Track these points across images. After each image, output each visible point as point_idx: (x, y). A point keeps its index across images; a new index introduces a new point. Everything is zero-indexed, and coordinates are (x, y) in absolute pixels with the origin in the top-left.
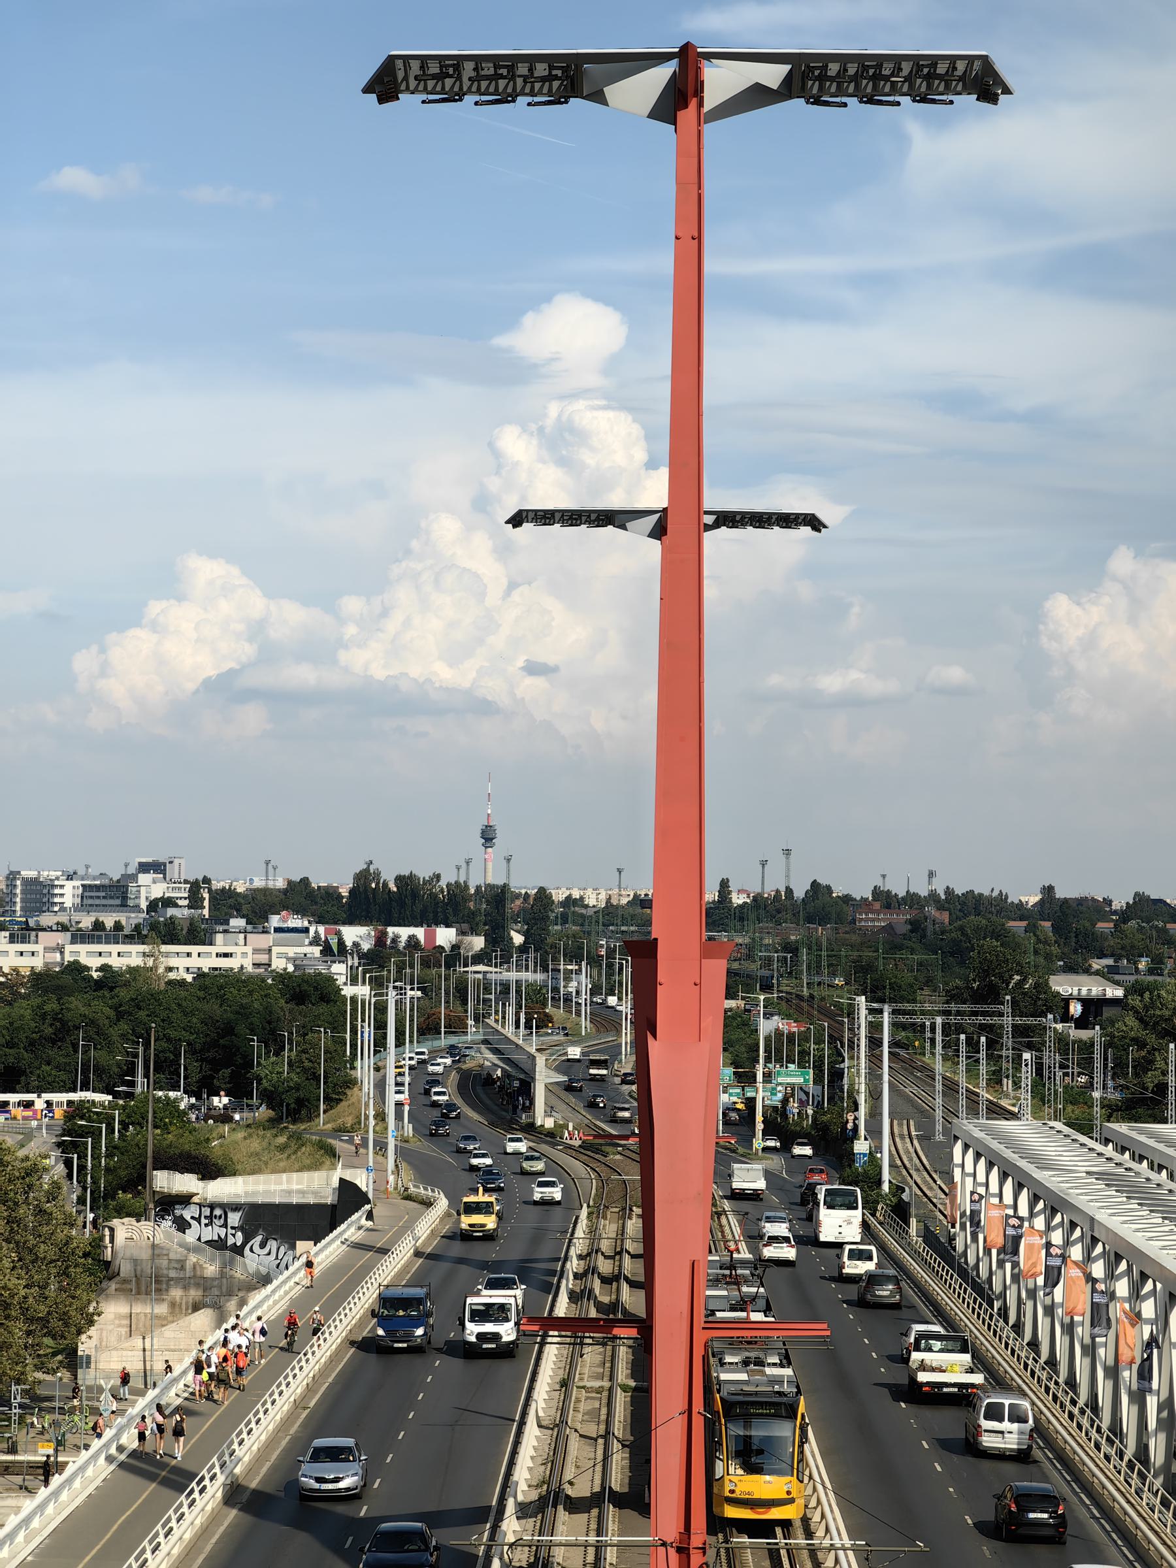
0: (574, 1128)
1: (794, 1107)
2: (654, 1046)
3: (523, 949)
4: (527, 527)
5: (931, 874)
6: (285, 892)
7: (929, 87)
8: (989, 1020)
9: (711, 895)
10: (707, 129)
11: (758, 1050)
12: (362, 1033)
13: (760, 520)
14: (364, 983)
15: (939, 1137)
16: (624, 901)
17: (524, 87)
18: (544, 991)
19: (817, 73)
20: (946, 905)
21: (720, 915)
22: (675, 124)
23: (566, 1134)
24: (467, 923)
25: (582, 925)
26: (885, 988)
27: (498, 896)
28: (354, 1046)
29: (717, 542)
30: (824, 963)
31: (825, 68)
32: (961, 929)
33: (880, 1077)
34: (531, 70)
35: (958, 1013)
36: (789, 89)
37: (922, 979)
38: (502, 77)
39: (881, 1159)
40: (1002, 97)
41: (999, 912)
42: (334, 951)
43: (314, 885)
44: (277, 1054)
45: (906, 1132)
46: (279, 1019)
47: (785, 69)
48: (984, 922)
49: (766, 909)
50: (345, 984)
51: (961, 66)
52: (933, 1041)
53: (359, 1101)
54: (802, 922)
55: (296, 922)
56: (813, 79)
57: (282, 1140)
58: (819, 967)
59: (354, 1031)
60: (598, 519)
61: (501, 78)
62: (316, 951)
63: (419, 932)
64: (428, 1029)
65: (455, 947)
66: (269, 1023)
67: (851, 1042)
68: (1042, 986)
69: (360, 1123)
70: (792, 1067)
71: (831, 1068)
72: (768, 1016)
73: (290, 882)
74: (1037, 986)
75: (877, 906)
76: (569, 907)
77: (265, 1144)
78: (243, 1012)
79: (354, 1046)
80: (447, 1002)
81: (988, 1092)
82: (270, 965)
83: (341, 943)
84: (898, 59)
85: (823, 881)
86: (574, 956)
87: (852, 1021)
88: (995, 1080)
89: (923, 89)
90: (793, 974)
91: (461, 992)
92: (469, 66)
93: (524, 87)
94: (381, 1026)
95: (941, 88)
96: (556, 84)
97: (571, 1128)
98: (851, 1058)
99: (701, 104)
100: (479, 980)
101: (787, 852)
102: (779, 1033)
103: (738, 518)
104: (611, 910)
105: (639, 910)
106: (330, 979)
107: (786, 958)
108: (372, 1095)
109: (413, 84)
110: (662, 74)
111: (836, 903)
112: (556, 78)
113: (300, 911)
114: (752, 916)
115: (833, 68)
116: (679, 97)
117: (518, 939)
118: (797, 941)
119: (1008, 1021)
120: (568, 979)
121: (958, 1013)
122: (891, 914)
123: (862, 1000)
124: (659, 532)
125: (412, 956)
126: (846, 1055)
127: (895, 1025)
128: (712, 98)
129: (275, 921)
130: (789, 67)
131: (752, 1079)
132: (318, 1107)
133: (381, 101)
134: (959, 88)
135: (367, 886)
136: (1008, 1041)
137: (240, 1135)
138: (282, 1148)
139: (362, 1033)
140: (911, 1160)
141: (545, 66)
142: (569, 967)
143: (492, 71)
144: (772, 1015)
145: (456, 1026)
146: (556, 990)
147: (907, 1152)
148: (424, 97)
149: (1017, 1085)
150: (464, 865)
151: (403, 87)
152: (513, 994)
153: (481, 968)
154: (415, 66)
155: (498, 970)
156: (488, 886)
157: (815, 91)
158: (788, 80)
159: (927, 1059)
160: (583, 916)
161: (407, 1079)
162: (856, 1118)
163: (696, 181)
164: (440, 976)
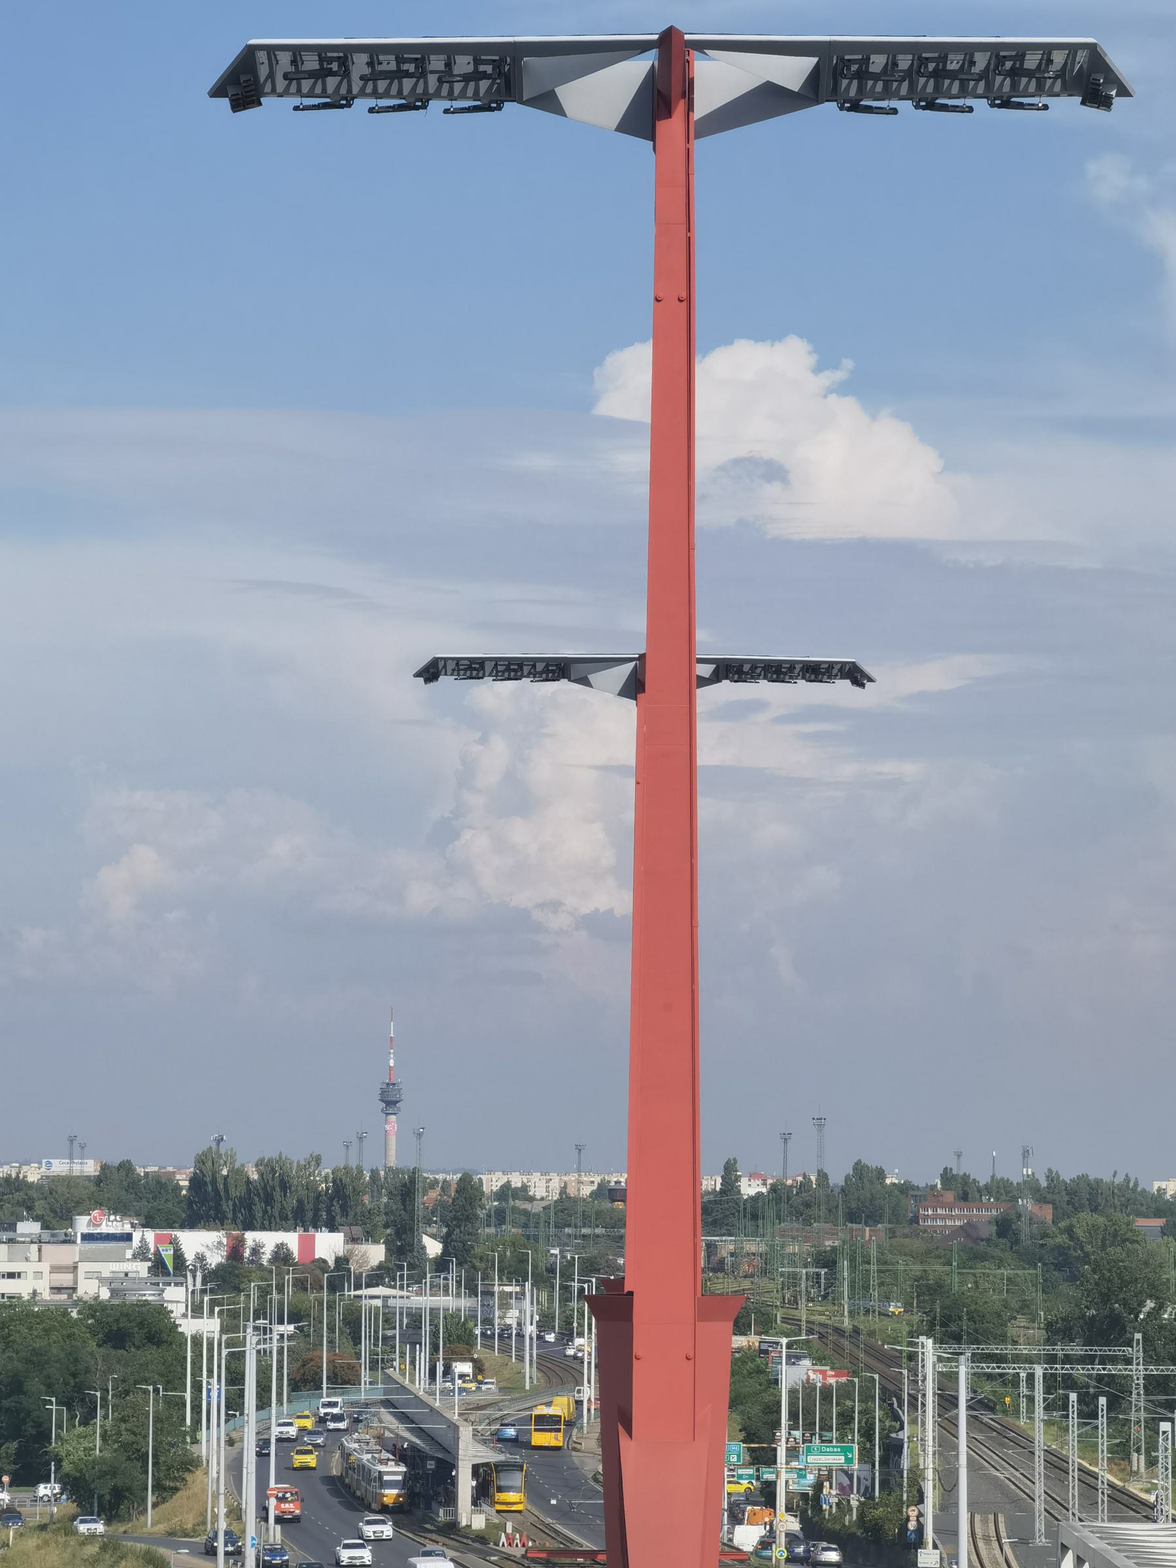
0: (515, 1529)
1: (830, 1494)
2: (628, 1448)
3: (441, 1264)
5: (1026, 1153)
6: (98, 1181)
7: (1014, 86)
9: (711, 1182)
10: (702, 147)
11: (779, 1412)
12: (209, 1391)
13: (777, 671)
15: (1041, 1541)
16: (586, 1191)
17: (439, 90)
18: (471, 1324)
19: (854, 68)
20: (1050, 1197)
21: (723, 1211)
23: (503, 1539)
25: (526, 1226)
26: (960, 1318)
27: (406, 1189)
28: (197, 1409)
34: (448, 65)
35: (1067, 1359)
36: (816, 90)
37: (1014, 1304)
38: (407, 74)
40: (1117, 101)
41: (1125, 1206)
42: (169, 1268)
43: (141, 1171)
44: (85, 1422)
46: (87, 1371)
47: (810, 62)
49: (790, 1204)
50: (185, 1316)
51: (1059, 58)
52: (1031, 1399)
53: (204, 1491)
54: (841, 1220)
55: (112, 1225)
56: (846, 76)
58: (866, 1288)
59: (197, 1387)
60: (546, 670)
62: (142, 1269)
63: (291, 1240)
64: (304, 1381)
65: (342, 1262)
66: (74, 1375)
67: (913, 1399)
69: (204, 1523)
71: (885, 1437)
72: (793, 1359)
73: (104, 1168)
75: (950, 1197)
76: (507, 1201)
77: (67, 1555)
78: (37, 1360)
79: (197, 1409)
80: (331, 1342)
81: (1110, 1471)
82: (74, 1289)
83: (179, 1257)
84: (969, 50)
85: (872, 1162)
86: (515, 1271)
87: (914, 1372)
88: (1121, 1452)
89: (1007, 88)
90: (828, 1296)
91: (352, 1323)
92: (361, 60)
93: (439, 90)
94: (235, 1378)
96: (484, 85)
97: (509, 1530)
98: (914, 1422)
99: (690, 107)
100: (377, 1308)
101: (820, 1122)
102: (809, 1387)
103: (746, 668)
105: (607, 1205)
106: (161, 1312)
107: (818, 1275)
109: (281, 84)
110: (636, 69)
111: (890, 1193)
112: (484, 75)
113: (119, 1208)
114: (771, 1213)
115: (878, 62)
116: (659, 103)
117: (433, 1248)
118: (834, 1249)
119: (1138, 1371)
120: (505, 1307)
121: (1067, 1359)
122: (969, 1209)
123: (929, 1343)
124: (634, 687)
125: (280, 1275)
126: (905, 1418)
127: (977, 1378)
128: (706, 101)
129: (82, 1224)
130: (815, 60)
131: (772, 1461)
132: (144, 1500)
136: (1138, 1398)
137: (32, 1542)
139: (209, 1391)
141: (470, 58)
142: (508, 1289)
143: (393, 66)
144: (798, 1358)
146: (488, 1321)
147: (1004, 1468)
148: (297, 101)
149: (1152, 1463)
150: (355, 1141)
151: (268, 88)
152: (426, 1328)
153: (380, 1291)
154: (285, 58)
155: (405, 1293)
156: (388, 1170)
157: (853, 93)
158: (814, 78)
159: (1022, 1422)
160: (526, 1213)
162: (920, 1515)
163: (684, 219)
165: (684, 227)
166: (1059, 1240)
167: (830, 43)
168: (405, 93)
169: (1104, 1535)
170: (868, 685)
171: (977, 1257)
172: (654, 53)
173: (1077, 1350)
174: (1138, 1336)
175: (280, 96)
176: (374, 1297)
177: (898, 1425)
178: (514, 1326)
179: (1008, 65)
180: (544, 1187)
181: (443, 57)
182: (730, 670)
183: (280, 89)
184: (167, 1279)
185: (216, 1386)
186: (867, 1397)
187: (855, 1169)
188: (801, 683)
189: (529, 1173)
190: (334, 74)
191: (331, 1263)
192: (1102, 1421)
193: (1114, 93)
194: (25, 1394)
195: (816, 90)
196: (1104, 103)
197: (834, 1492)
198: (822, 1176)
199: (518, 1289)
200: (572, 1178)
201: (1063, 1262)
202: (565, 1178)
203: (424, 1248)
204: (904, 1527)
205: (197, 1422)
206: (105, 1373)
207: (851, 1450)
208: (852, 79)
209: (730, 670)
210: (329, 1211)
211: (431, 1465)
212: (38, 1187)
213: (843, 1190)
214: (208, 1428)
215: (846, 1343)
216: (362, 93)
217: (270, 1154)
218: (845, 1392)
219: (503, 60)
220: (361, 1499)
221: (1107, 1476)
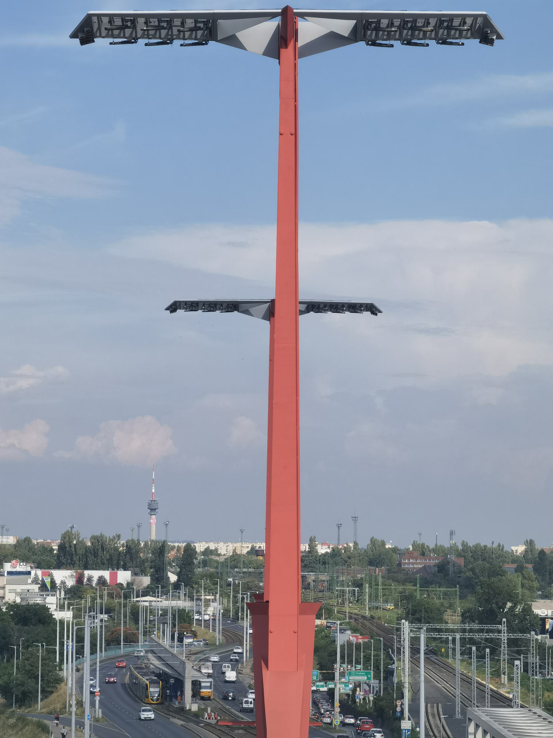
0: (212, 711)
1: (360, 694)
2: (267, 675)
3: (177, 586)
4: (180, 312)
5: (452, 533)
6: (15, 546)
8: (492, 635)
10: (301, 62)
12: (67, 646)
14: (69, 609)
16: (245, 551)
21: (310, 561)
22: (279, 58)
23: (206, 716)
24: (139, 570)
25: (217, 568)
26: (421, 611)
27: (161, 550)
28: (61, 654)
29: (308, 321)
30: (380, 593)
31: (379, 22)
32: (472, 570)
33: (419, 672)
35: (471, 631)
36: (356, 36)
38: (163, 28)
39: (419, 732)
45: (436, 712)
47: (353, 22)
48: (487, 565)
50: (56, 610)
51: (469, 21)
52: (454, 650)
53: (65, 693)
55: (21, 567)
56: (369, 30)
57: (12, 721)
58: (377, 597)
59: (62, 644)
61: (163, 29)
62: (36, 588)
63: (106, 574)
64: (113, 641)
67: (399, 649)
68: (528, 610)
69: (65, 707)
70: (359, 667)
72: (342, 631)
74: (524, 610)
75: (416, 554)
79: (61, 654)
80: (125, 622)
83: (53, 583)
84: (427, 18)
87: (399, 636)
92: (142, 21)
94: (80, 640)
95: (457, 35)
96: (200, 33)
97: (209, 711)
99: (296, 40)
101: (355, 519)
103: (321, 306)
104: (236, 557)
106: (44, 609)
107: (354, 591)
108: (74, 693)
109: (104, 33)
110: (272, 25)
112: (200, 28)
113: (24, 559)
116: (284, 38)
117: (173, 578)
118: (362, 578)
119: (504, 637)
121: (471, 631)
122: (425, 560)
126: (395, 658)
127: (429, 640)
133: (83, 42)
134: (469, 35)
135: (70, 542)
136: (504, 648)
138: (13, 727)
139: (67, 646)
140: (439, 732)
141: (193, 20)
142: (208, 597)
143: (157, 24)
144: (345, 630)
145: (131, 639)
147: (437, 727)
149: (511, 679)
150: (136, 528)
153: (148, 598)
154: (105, 20)
155: (159, 599)
158: (355, 29)
159: (450, 660)
160: (217, 562)
161: (98, 689)
164: (120, 604)
165: (294, 100)
166: (468, 574)
167: (362, 14)
170: (379, 314)
173: (476, 626)
174: (504, 620)
175: (104, 37)
176: (146, 601)
179: (445, 24)
180: (225, 549)
183: (103, 35)
184: (48, 593)
185: (71, 644)
186: (377, 649)
187: (371, 541)
188: (347, 313)
190: (129, 28)
191: (125, 585)
193: (495, 37)
196: (490, 42)
197: (362, 693)
199: (213, 597)
200: (238, 545)
202: (235, 545)
204: (395, 711)
206: (18, 638)
207: (370, 674)
210: (123, 561)
211: (172, 681)
214: (67, 663)
216: (142, 37)
218: (367, 646)
219: (208, 21)
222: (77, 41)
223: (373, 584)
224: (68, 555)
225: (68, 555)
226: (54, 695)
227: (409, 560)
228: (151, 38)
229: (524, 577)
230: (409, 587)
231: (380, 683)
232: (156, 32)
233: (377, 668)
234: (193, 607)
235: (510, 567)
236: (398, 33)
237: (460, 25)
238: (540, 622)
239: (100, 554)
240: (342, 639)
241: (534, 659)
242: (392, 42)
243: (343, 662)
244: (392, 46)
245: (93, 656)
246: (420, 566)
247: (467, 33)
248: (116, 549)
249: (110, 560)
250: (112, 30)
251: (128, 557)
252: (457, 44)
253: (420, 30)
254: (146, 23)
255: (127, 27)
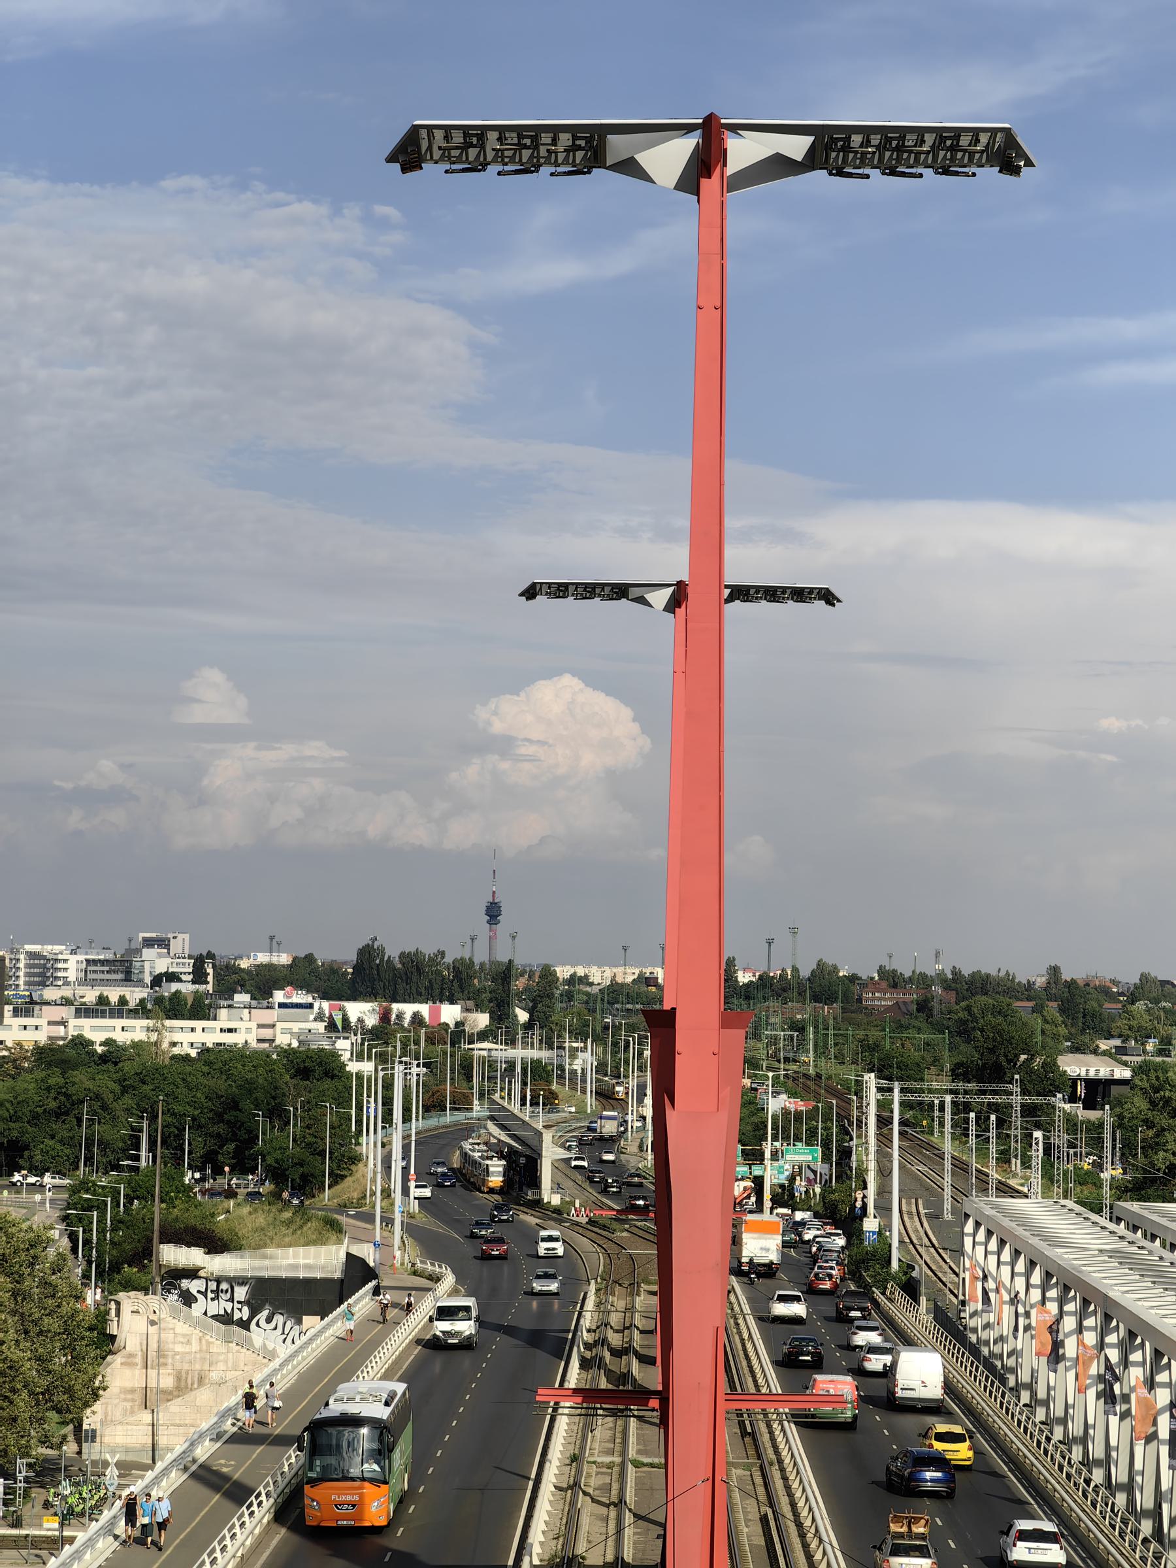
1: (800, 1185)
2: (671, 1116)
3: (528, 1026)
5: (937, 954)
8: (998, 1099)
12: (368, 1108)
15: (948, 1217)
16: (629, 979)
22: (698, 195)
27: (504, 974)
28: (359, 1122)
35: (966, 1092)
36: (812, 161)
38: (526, 147)
45: (914, 1210)
46: (284, 1095)
47: (808, 140)
50: (351, 1060)
52: (942, 1124)
54: (808, 1001)
58: (825, 1046)
59: (359, 1108)
62: (321, 1027)
63: (424, 1009)
64: (433, 1105)
66: (274, 1098)
67: (859, 1121)
68: (1051, 1066)
69: (364, 1197)
70: (799, 1145)
72: (776, 1094)
73: (295, 959)
74: (1045, 1065)
75: (884, 985)
77: (270, 1219)
78: (249, 1087)
79: (359, 1122)
82: (273, 1040)
83: (345, 1020)
84: (921, 131)
85: (830, 961)
86: (580, 1033)
88: (1004, 1158)
91: (466, 1069)
94: (388, 1102)
96: (580, 155)
97: (577, 1205)
98: (859, 1136)
99: (725, 165)
100: (484, 1057)
101: (794, 931)
102: (786, 1112)
106: (335, 1055)
107: (792, 1037)
108: (379, 1169)
109: (437, 154)
110: (683, 148)
112: (580, 148)
116: (705, 162)
117: (523, 1016)
118: (804, 1020)
119: (1017, 1100)
120: (573, 1056)
121: (966, 1092)
129: (279, 996)
133: (404, 170)
136: (1017, 1119)
137: (246, 1210)
139: (368, 1108)
141: (569, 136)
144: (778, 1093)
145: (461, 1103)
152: (519, 1069)
153: (486, 1045)
155: (503, 1047)
158: (812, 151)
160: (588, 994)
162: (864, 1197)
163: (719, 251)
164: (445, 1053)
165: (719, 256)
166: (961, 1015)
167: (823, 126)
168: (524, 160)
169: (995, 1207)
170: (837, 604)
171: (900, 1027)
172: (699, 132)
173: (972, 1086)
174: (1017, 1077)
175: (436, 162)
176: (482, 1049)
177: (848, 1138)
178: (579, 1071)
179: (949, 143)
180: (600, 976)
181: (551, 135)
182: (741, 593)
183: (436, 157)
184: (338, 1035)
185: (372, 1105)
186: (827, 1119)
187: (818, 965)
188: (790, 602)
189: (589, 966)
190: (475, 146)
191: (452, 1025)
192: (992, 1133)
193: (1022, 163)
194: (240, 1110)
195: (812, 161)
196: (1015, 171)
197: (803, 1183)
198: (795, 970)
199: (582, 1045)
200: (619, 970)
201: (964, 1031)
202: (615, 970)
203: (516, 1016)
204: (853, 1207)
205: (359, 1132)
206: (295, 1097)
207: (816, 1151)
208: (839, 152)
209: (741, 593)
210: (450, 990)
211: (523, 1160)
212: (247, 972)
213: (809, 979)
214: (368, 1134)
215: (811, 1084)
216: (494, 161)
217: (410, 949)
218: (812, 1114)
219: (592, 137)
220: (473, 1184)
221: (994, 1175)
222: (397, 166)
223: (820, 1025)
224: (372, 976)
225: (372, 976)
226: (349, 1180)
227: (873, 993)
228: (506, 164)
229: (1046, 1021)
230: (875, 1033)
231: (831, 1170)
232: (514, 154)
233: (826, 1147)
234: (552, 1059)
235: (1022, 1006)
236: (877, 156)
237: (970, 145)
238: (1070, 1083)
239: (414, 980)
240: (776, 1104)
241: (1060, 1139)
242: (867, 171)
243: (775, 1138)
244: (868, 177)
245: (407, 1125)
246: (890, 1003)
247: (981, 157)
248: (439, 973)
249: (430, 988)
250: (449, 149)
251: (456, 984)
252: (966, 175)
253: (911, 152)
254: (500, 139)
255: (472, 146)
